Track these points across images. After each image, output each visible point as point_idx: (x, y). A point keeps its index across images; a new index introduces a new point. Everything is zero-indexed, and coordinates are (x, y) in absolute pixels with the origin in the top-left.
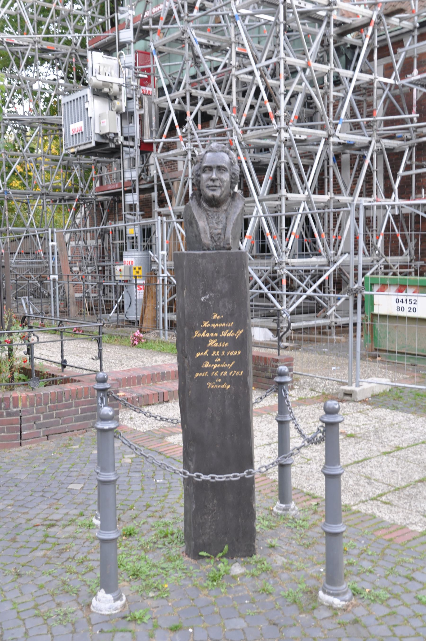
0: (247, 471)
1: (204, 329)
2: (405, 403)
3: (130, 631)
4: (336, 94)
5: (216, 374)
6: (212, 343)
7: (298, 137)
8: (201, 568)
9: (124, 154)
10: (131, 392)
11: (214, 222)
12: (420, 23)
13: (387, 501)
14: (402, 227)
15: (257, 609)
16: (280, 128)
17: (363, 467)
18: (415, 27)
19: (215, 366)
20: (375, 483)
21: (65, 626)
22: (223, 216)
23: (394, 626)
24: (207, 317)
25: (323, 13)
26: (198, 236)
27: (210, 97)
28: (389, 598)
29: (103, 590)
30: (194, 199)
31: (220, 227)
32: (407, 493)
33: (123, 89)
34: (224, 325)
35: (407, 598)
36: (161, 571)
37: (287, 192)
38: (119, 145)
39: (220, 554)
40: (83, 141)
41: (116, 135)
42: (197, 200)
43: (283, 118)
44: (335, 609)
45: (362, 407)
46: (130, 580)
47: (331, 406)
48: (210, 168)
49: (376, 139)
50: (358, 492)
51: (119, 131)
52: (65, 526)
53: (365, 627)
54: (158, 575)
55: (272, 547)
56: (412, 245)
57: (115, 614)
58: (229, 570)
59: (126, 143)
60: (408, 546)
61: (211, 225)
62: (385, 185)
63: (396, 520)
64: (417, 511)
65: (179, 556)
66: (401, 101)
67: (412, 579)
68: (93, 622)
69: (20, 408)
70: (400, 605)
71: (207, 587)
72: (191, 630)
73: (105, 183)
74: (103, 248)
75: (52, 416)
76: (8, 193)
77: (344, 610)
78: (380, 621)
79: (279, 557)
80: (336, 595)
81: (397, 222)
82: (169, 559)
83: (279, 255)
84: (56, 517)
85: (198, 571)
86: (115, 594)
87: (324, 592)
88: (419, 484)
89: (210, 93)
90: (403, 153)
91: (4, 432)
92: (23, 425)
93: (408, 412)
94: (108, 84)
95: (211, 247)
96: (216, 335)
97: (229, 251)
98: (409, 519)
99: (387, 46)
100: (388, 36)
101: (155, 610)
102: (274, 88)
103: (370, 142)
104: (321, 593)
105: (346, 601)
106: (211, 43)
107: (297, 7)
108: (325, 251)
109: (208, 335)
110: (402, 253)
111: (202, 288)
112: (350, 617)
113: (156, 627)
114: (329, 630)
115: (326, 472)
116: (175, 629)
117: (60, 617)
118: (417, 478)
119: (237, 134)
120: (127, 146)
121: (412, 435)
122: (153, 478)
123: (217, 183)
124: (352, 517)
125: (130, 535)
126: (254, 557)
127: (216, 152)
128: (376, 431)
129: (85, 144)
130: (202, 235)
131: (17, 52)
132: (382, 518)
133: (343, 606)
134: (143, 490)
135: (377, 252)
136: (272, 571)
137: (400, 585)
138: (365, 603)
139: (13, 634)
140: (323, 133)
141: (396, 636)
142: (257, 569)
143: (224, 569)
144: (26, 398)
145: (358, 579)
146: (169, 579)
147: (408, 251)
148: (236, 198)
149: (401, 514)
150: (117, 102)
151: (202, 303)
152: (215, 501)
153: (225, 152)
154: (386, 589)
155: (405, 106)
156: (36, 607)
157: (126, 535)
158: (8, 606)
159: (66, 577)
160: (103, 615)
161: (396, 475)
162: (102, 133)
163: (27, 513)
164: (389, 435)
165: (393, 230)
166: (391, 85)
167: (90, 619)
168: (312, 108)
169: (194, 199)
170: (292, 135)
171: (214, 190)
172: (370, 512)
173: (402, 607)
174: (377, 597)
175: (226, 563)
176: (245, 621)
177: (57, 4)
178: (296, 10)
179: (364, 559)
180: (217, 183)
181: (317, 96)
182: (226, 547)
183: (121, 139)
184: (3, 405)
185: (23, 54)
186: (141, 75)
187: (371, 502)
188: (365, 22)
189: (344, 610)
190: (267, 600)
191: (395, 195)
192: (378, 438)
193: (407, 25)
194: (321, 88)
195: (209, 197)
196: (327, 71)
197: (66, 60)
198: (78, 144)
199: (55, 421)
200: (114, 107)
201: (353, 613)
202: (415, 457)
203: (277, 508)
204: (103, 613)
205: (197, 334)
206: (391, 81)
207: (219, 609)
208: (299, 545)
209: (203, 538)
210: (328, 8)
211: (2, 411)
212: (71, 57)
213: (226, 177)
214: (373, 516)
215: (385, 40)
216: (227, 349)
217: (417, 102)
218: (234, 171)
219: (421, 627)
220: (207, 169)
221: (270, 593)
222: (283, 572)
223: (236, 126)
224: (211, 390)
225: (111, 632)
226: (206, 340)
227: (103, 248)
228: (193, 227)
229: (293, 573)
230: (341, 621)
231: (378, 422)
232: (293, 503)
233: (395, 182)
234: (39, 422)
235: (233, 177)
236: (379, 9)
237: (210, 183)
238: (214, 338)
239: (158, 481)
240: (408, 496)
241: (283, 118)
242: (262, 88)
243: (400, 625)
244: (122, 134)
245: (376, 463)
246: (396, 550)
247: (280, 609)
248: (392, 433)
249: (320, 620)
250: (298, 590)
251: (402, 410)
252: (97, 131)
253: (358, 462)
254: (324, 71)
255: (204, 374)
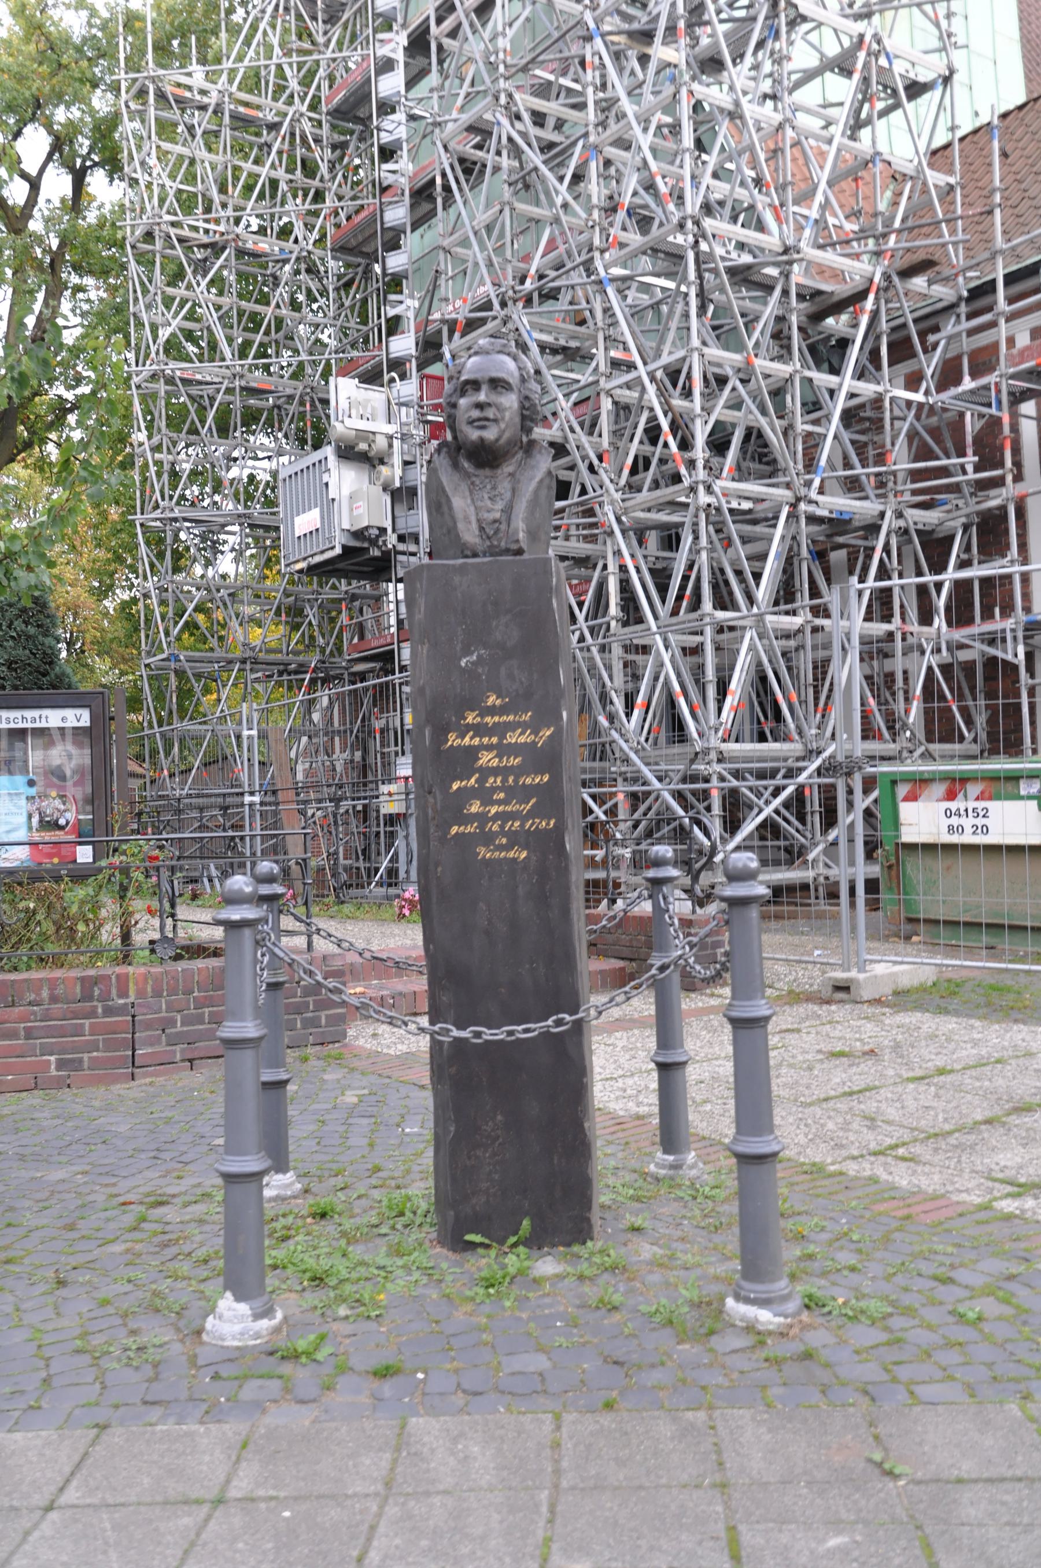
0: (554, 1018)
1: (469, 727)
2: (965, 1003)
3: (280, 1377)
4: (809, 428)
5: (495, 828)
6: (486, 759)
7: (734, 505)
8: (467, 1266)
9: (399, 568)
10: (381, 988)
11: (486, 496)
12: (969, 291)
13: (907, 1155)
14: (960, 688)
15: (582, 1336)
16: (697, 483)
17: (860, 1102)
18: (960, 298)
19: (494, 810)
20: (885, 1126)
21: (137, 1368)
22: (505, 487)
23: (896, 1363)
24: (473, 703)
25: (772, 271)
26: (452, 531)
27: (559, 440)
28: (891, 1315)
29: (228, 1294)
30: (443, 455)
31: (500, 505)
32: (955, 1142)
33: (396, 443)
34: (511, 718)
35: (931, 1315)
36: (376, 1272)
37: (715, 608)
38: (389, 552)
39: (513, 1240)
40: (318, 546)
41: (383, 531)
42: (450, 457)
43: (700, 464)
44: (759, 1333)
45: (870, 1010)
46: (304, 1290)
47: (740, 865)
48: (474, 385)
49: (894, 507)
50: (844, 1142)
51: (388, 524)
52: (186, 1205)
53: (827, 1365)
54: (367, 1279)
55: (636, 1230)
56: (981, 720)
57: (255, 1346)
58: (529, 1268)
59: (401, 547)
60: (946, 1226)
61: (479, 504)
62: (919, 608)
63: (923, 1187)
64: (973, 1171)
65: (421, 1245)
66: (943, 441)
67: (951, 1281)
68: (201, 1362)
69: (132, 999)
70: (913, 1327)
71: (473, 1299)
72: (420, 1376)
73: (368, 636)
74: (364, 766)
75: (200, 1020)
76: (177, 660)
77: (782, 1334)
78: (865, 1355)
79: (648, 1246)
80: (763, 1303)
81: (948, 679)
82: (397, 1252)
83: (701, 735)
84: (171, 1190)
85: (458, 1270)
86: (258, 1303)
87: (738, 1298)
88: (983, 1127)
89: (560, 434)
90: (951, 538)
91: (97, 1050)
92: (137, 1035)
93: (969, 1016)
94: (368, 436)
95: (480, 549)
96: (495, 740)
97: (518, 558)
98: (953, 1183)
99: (908, 339)
100: (910, 318)
101: (348, 1341)
102: (685, 416)
103: (882, 515)
104: (730, 1302)
105: (786, 1317)
106: (562, 342)
107: (723, 259)
108: (800, 733)
109: (476, 741)
110: (962, 739)
111: (460, 638)
112: (795, 1347)
113: (343, 1369)
114: (742, 1372)
115: (735, 1014)
116: (384, 1373)
117: (129, 1353)
118: (979, 1117)
119: (612, 502)
120: (403, 553)
121: (975, 1051)
122: (398, 1126)
123: (490, 413)
124: (826, 1182)
125: (323, 1215)
126: (589, 1244)
127: (488, 353)
128: (897, 1046)
129: (322, 552)
130: (461, 526)
131: (202, 397)
132: (893, 1183)
133: (779, 1325)
134: (371, 1145)
135: (908, 734)
136: (625, 1269)
137: (918, 1291)
138: (833, 1323)
139: (16, 1383)
140: (785, 494)
141: (899, 1382)
142: (591, 1265)
143: (518, 1265)
144: (145, 977)
145: (823, 1282)
146: (389, 1285)
147: (973, 735)
148: (535, 452)
149: (936, 1177)
150: (384, 470)
151: (463, 671)
152: (499, 1117)
153: (509, 354)
154: (885, 1298)
155: (950, 445)
156: (84, 1335)
157: (314, 1216)
158: (20, 1336)
159: (164, 1285)
160: (228, 1347)
161: (932, 1113)
162: (354, 529)
163: (114, 1185)
164: (924, 1052)
165: (942, 697)
166: (920, 406)
167: (195, 1356)
168: (768, 463)
169: (443, 455)
170: (723, 500)
171: (483, 427)
172: (867, 1173)
173: (919, 1330)
174: (862, 1312)
175: (522, 1256)
176: (550, 1359)
177: (278, 306)
178: (721, 265)
179: (842, 1248)
180: (490, 413)
181: (773, 430)
182: (526, 1223)
183: (392, 539)
184: (97, 992)
185: (212, 399)
186: (430, 418)
187: (872, 1159)
188: (861, 288)
189: (782, 1335)
190: (606, 1322)
191: (939, 621)
192: (902, 1057)
193: (943, 293)
194: (780, 417)
195: (473, 442)
196: (787, 376)
197: (292, 409)
198: (309, 553)
199: (206, 1030)
200: (378, 479)
201: (801, 1340)
202: (978, 1084)
203: (657, 1165)
204: (226, 1343)
205: (453, 740)
206: (918, 397)
207: (494, 1337)
208: (697, 1227)
209: (474, 1201)
210: (785, 258)
211: (95, 1003)
212: (302, 403)
213: (510, 401)
214: (873, 1180)
215: (904, 325)
216: (518, 771)
217: (974, 443)
218: (527, 393)
219: (958, 1365)
220: (468, 387)
221: (615, 1308)
222: (651, 1272)
223: (611, 487)
224: (486, 863)
225: (236, 1378)
226: (472, 753)
227: (364, 766)
228: (442, 514)
229: (675, 1273)
230: (771, 1355)
231: (903, 1033)
232: (693, 1154)
233: (939, 596)
234: (173, 1030)
235: (527, 405)
236: (886, 262)
237: (476, 414)
238: (489, 748)
239: (408, 1130)
240: (956, 1147)
241: (700, 464)
242: (665, 424)
243: (911, 1362)
244: (394, 531)
245: (889, 1095)
246: (918, 1234)
247: (635, 1336)
248: (931, 1048)
249: (724, 1354)
250: (680, 1302)
251: (957, 1013)
252: (346, 526)
253: (851, 1094)
254: (782, 375)
255: (470, 829)
